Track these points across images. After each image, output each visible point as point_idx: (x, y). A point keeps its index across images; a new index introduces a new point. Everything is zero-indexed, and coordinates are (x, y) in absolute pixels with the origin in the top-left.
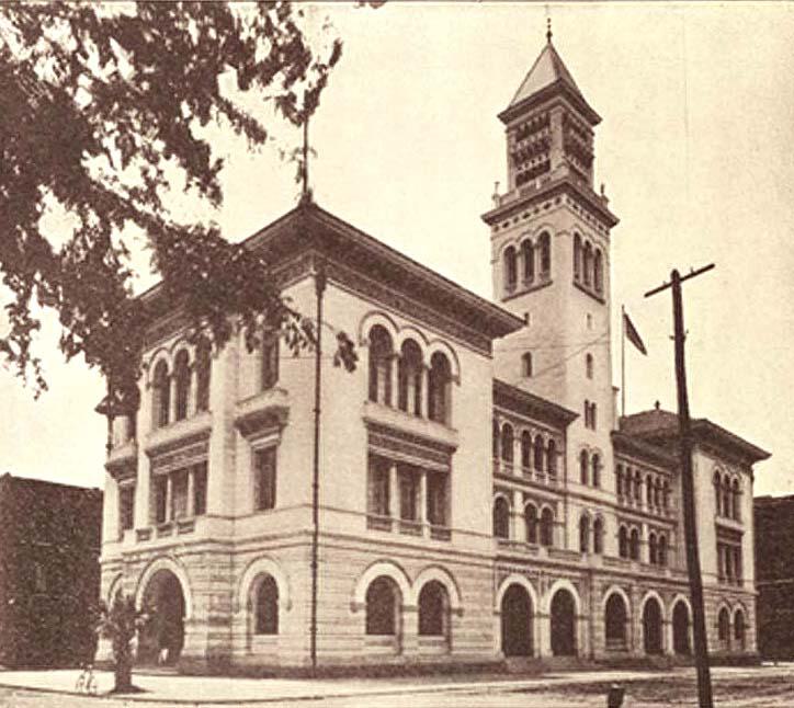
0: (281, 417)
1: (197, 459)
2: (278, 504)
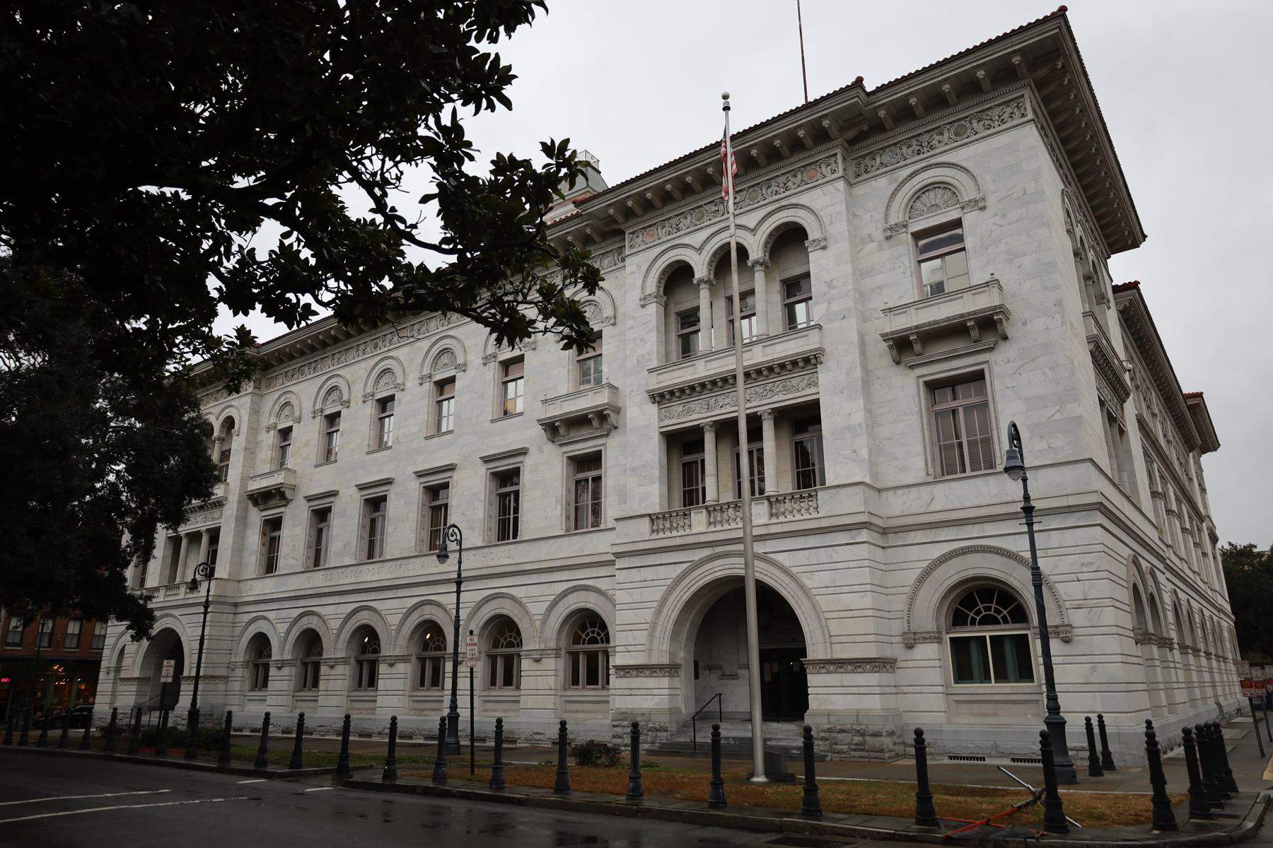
0: (613, 417)
1: (211, 524)
2: (524, 533)
